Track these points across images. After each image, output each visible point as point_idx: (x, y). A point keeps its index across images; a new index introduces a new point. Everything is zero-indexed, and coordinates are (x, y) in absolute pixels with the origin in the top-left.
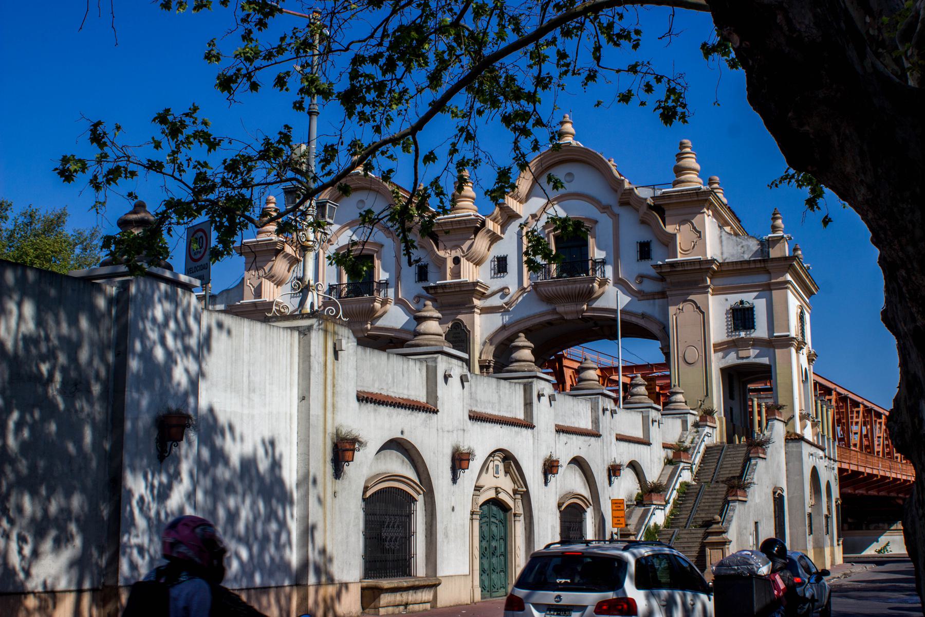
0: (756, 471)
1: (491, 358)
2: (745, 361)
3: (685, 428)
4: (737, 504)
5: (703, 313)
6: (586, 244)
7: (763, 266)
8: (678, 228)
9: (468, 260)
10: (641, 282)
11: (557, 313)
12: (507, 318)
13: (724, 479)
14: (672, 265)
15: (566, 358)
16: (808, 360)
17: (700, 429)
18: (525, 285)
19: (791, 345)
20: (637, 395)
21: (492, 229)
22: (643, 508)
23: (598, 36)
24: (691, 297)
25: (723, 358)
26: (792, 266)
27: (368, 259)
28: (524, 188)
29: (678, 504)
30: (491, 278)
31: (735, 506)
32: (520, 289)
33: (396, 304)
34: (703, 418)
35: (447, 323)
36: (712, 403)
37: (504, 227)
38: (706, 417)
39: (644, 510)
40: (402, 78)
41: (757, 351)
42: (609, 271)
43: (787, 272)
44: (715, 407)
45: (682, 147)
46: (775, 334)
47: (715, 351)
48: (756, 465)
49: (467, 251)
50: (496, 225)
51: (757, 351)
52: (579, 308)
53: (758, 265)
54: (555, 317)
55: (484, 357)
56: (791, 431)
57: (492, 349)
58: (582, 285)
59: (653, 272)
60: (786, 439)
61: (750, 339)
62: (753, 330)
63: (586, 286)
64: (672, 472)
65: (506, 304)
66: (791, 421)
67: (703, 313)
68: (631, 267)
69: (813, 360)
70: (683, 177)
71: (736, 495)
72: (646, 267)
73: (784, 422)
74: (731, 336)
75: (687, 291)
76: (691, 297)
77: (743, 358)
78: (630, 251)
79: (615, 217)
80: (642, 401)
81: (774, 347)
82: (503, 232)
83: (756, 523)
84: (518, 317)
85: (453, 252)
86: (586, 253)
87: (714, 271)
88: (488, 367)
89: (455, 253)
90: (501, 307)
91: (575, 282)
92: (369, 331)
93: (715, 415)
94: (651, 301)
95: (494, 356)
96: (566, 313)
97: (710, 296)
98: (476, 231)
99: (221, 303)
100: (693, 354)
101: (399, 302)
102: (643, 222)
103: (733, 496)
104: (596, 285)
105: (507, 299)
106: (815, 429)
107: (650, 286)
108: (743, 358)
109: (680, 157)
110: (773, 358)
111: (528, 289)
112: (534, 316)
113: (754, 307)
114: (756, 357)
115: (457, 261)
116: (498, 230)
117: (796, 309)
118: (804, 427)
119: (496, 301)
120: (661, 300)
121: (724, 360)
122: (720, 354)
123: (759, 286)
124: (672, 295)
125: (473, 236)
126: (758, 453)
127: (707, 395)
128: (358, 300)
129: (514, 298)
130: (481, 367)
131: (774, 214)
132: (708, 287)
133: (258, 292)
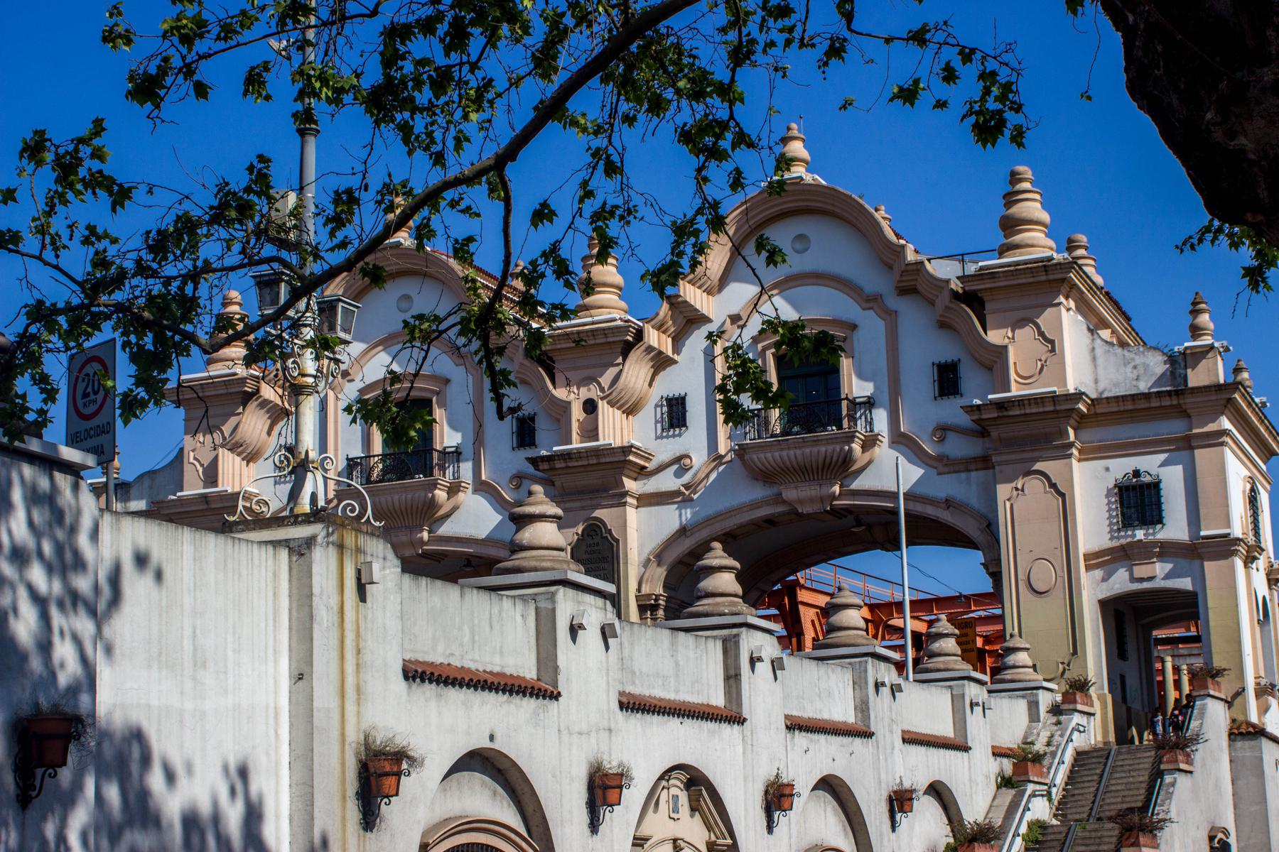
0: (1174, 797)
1: (659, 590)
2: (1146, 585)
3: (1034, 716)
7: (1175, 402)
8: (1010, 335)
9: (611, 404)
11: (784, 502)
12: (688, 514)
13: (1113, 813)
14: (1001, 405)
15: (803, 587)
16: (1269, 580)
17: (1063, 718)
19: (1235, 553)
21: (656, 345)
24: (1038, 466)
25: (1104, 580)
26: (1230, 401)
27: (419, 407)
30: (657, 438)
33: (475, 491)
34: (1068, 697)
37: (678, 340)
38: (1075, 694)
41: (1169, 566)
42: (881, 419)
43: (1222, 413)
44: (1091, 675)
45: (1015, 178)
46: (1203, 533)
47: (1088, 568)
48: (1173, 784)
49: (610, 387)
50: (663, 336)
51: (1169, 566)
52: (825, 491)
53: (1166, 402)
54: (780, 509)
55: (646, 589)
56: (1240, 718)
57: (661, 572)
60: (1231, 734)
62: (1159, 526)
65: (687, 487)
67: (1062, 495)
70: (1017, 238)
72: (951, 409)
73: (1226, 701)
74: (1118, 538)
76: (1038, 466)
77: (1141, 580)
78: (920, 381)
79: (890, 316)
80: (951, 666)
81: (1202, 558)
85: (583, 390)
88: (654, 608)
89: (585, 393)
90: (677, 493)
91: (817, 442)
92: (426, 544)
94: (963, 475)
95: (666, 587)
96: (801, 501)
97: (1074, 462)
98: (626, 349)
99: (140, 498)
100: (1045, 575)
101: (482, 487)
102: (943, 325)
104: (856, 447)
105: (687, 478)
107: (958, 447)
108: (1141, 580)
109: (1011, 198)
110: (1201, 579)
111: (728, 458)
112: (740, 509)
113: (1160, 481)
115: (590, 407)
116: (667, 346)
119: (667, 482)
120: (981, 473)
121: (1104, 584)
122: (1098, 573)
124: (1001, 463)
127: (1075, 652)
128: (404, 487)
130: (642, 609)
131: (1195, 304)
132: (1071, 445)
133: (211, 475)
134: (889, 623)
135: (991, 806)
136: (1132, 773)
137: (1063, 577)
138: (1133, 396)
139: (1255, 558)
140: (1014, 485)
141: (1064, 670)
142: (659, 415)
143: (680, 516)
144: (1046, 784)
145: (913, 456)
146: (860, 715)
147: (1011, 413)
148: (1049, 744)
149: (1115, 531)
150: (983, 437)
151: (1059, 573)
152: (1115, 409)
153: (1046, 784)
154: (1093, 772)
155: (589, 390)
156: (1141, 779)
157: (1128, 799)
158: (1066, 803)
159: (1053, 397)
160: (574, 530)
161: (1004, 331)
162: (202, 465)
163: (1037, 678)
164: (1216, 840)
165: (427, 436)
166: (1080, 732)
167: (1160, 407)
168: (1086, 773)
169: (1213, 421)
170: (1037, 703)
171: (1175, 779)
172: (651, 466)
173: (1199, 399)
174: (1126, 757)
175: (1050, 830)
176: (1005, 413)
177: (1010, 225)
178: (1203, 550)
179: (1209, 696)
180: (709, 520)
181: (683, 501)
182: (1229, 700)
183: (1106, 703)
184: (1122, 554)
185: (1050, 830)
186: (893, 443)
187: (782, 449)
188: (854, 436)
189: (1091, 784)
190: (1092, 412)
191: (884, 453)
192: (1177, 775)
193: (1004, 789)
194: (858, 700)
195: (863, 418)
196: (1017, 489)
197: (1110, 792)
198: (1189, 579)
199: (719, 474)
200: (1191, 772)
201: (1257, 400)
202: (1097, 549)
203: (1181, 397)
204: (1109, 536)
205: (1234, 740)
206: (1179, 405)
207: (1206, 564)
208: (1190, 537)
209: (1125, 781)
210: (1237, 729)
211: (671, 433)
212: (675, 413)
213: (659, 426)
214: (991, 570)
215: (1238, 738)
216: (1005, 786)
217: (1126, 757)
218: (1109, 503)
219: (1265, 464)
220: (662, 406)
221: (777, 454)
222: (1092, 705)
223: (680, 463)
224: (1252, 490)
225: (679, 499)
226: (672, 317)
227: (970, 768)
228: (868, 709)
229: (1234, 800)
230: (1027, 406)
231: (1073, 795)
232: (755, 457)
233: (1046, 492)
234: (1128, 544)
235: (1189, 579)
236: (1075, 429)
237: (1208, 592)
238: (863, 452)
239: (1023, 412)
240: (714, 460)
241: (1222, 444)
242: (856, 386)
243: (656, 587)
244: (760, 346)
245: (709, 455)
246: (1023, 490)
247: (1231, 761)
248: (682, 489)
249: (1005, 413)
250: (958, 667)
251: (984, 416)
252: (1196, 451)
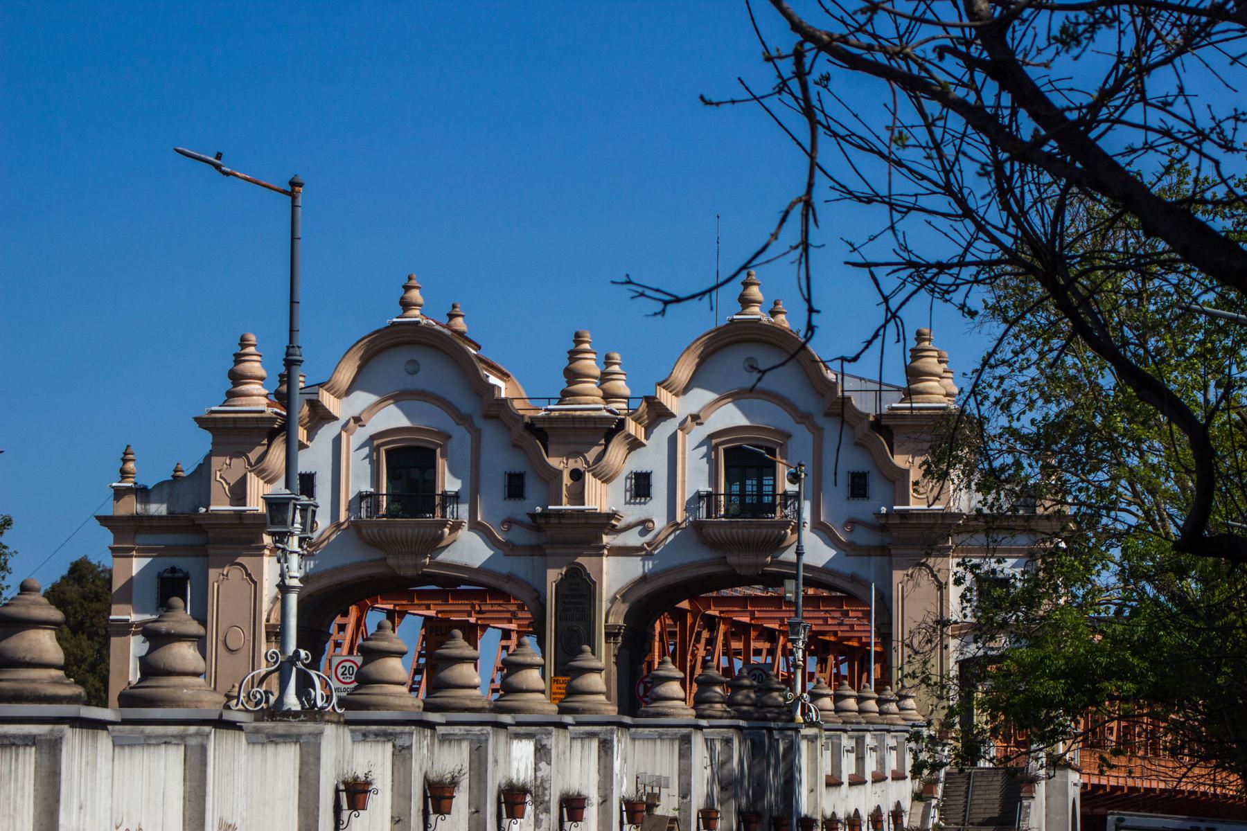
1: (621, 623)
6: (433, 466)
8: (911, 460)
9: (595, 476)
11: (726, 564)
12: (649, 565)
13: (980, 820)
18: (679, 520)
21: (633, 433)
23: (899, 163)
24: (239, 560)
28: (685, 376)
30: (626, 503)
32: (671, 524)
33: (470, 529)
35: (561, 568)
40: (890, 192)
42: (463, 510)
45: (243, 343)
46: (111, 617)
48: (1029, 807)
50: (639, 426)
54: (722, 569)
55: (611, 621)
57: (623, 608)
58: (770, 531)
59: (870, 518)
63: (433, 531)
65: (649, 544)
67: (255, 583)
68: (495, 504)
70: (921, 386)
72: (518, 509)
76: (239, 560)
78: (494, 485)
79: (817, 431)
82: (647, 437)
84: (667, 565)
85: (571, 461)
86: (432, 483)
88: (616, 635)
89: (573, 464)
90: (641, 548)
91: (760, 525)
92: (426, 567)
94: (865, 559)
95: (625, 620)
97: (266, 559)
98: (609, 435)
99: (161, 502)
100: (238, 638)
101: (475, 526)
102: (515, 446)
104: (447, 530)
105: (649, 537)
107: (863, 537)
109: (239, 358)
111: (684, 525)
115: (577, 475)
119: (632, 539)
120: (879, 558)
125: (603, 441)
128: (419, 524)
129: (661, 537)
130: (608, 635)
131: (125, 454)
142: (628, 486)
143: (644, 566)
145: (829, 541)
155: (576, 462)
156: (995, 797)
157: (988, 811)
160: (559, 571)
161: (907, 456)
162: (228, 484)
165: (431, 482)
172: (619, 525)
177: (237, 378)
180: (666, 572)
191: (810, 539)
199: (675, 537)
211: (638, 501)
212: (641, 486)
213: (628, 494)
220: (631, 478)
221: (728, 531)
223: (645, 525)
226: (648, 413)
232: (711, 531)
233: (243, 579)
242: (449, 483)
243: (618, 619)
244: (714, 442)
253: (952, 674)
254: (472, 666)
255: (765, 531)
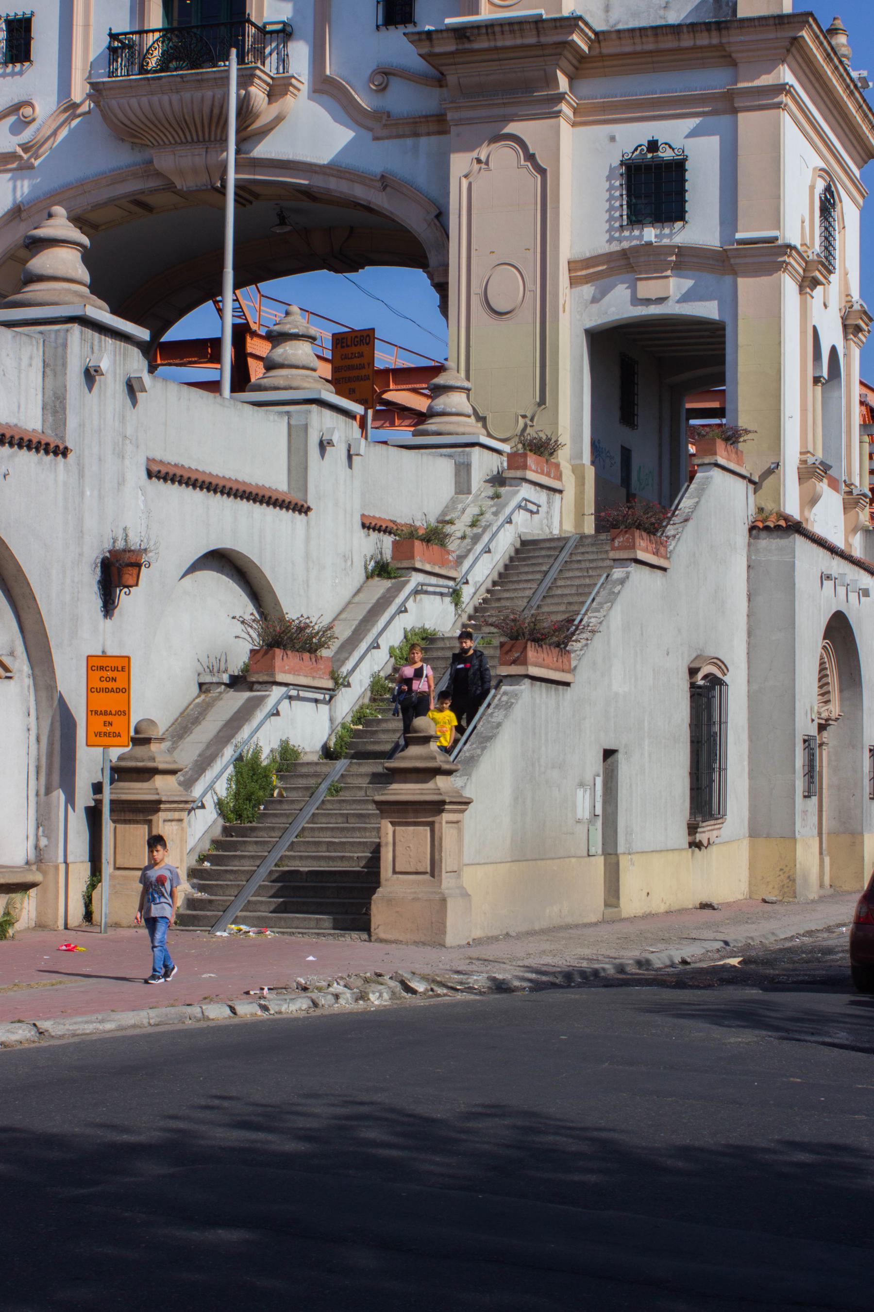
0: (620, 599)
2: (654, 310)
3: (463, 486)
4: (525, 686)
5: (542, 171)
7: (715, 41)
10: (382, 89)
11: (158, 174)
14: (461, 33)
15: (254, 334)
16: (845, 327)
17: (503, 490)
19: (781, 267)
20: (282, 366)
22: (247, 694)
25: (595, 300)
26: (796, 41)
29: (383, 687)
31: (516, 695)
32: (65, 103)
34: (516, 461)
36: (556, 423)
38: (525, 455)
39: (249, 700)
41: (688, 283)
43: (783, 61)
44: (565, 436)
46: (739, 236)
47: (574, 282)
48: (622, 582)
51: (688, 283)
53: (703, 40)
54: (152, 184)
56: (769, 506)
60: (752, 529)
61: (669, 250)
62: (679, 224)
64: (383, 597)
65: (26, 148)
66: (771, 479)
69: (858, 329)
71: (522, 661)
73: (751, 481)
74: (620, 240)
75: (496, 111)
76: (512, 128)
77: (648, 302)
80: (295, 384)
81: (735, 272)
83: (609, 754)
87: (582, 58)
93: (563, 457)
94: (409, 142)
97: (564, 126)
103: (514, 662)
105: (27, 135)
106: (852, 513)
108: (648, 302)
110: (731, 303)
111: (85, 108)
113: (685, 160)
114: (685, 298)
117: (809, 174)
118: (811, 500)
120: (434, 139)
121: (595, 307)
122: (588, 290)
123: (702, 100)
124: (460, 123)
126: (633, 547)
127: (542, 402)
132: (560, 98)
134: (385, 396)
135: (349, 603)
136: (591, 573)
137: (534, 292)
138: (655, 29)
139: (815, 283)
140: (474, 154)
141: (526, 426)
143: (14, 189)
144: (454, 579)
146: (50, 419)
147: (476, 46)
148: (473, 525)
149: (616, 230)
150: (441, 86)
151: (529, 286)
152: (628, 49)
153: (454, 579)
154: (537, 569)
158: (485, 610)
159: (536, 22)
163: (471, 429)
164: (700, 675)
166: (531, 512)
167: (694, 48)
168: (526, 569)
169: (769, 72)
170: (468, 466)
171: (628, 573)
173: (747, 38)
174: (590, 549)
175: (440, 644)
176: (467, 46)
178: (738, 261)
179: (717, 465)
181: (20, 168)
182: (756, 479)
183: (583, 478)
184: (623, 262)
185: (440, 644)
186: (315, 91)
187: (152, 93)
188: (253, 76)
189: (529, 585)
190: (596, 52)
192: (633, 568)
193: (377, 579)
194: (49, 393)
195: (274, 55)
196: (479, 161)
197: (552, 596)
198: (715, 304)
199: (70, 131)
200: (664, 569)
201: (854, 74)
202: (588, 255)
203: (724, 32)
204: (607, 236)
205: (757, 538)
206: (721, 46)
207: (740, 281)
208: (722, 241)
209: (577, 582)
210: (763, 521)
214: (436, 281)
215: (763, 534)
216: (379, 575)
217: (590, 549)
218: (611, 188)
219: (859, 168)
221: (144, 100)
222: (559, 477)
224: (828, 189)
225: (14, 166)
227: (308, 539)
228: (64, 409)
229: (748, 623)
230: (499, 35)
231: (499, 600)
232: (114, 103)
234: (631, 248)
235: (715, 304)
236: (571, 79)
237: (740, 322)
238: (270, 103)
239: (492, 44)
240: (65, 110)
241: (778, 106)
245: (59, 102)
246: (487, 163)
247: (749, 567)
248: (19, 151)
249: (467, 46)
250: (306, 385)
251: (438, 50)
252: (741, 116)
253: (464, 645)
254: (464, 396)
255: (209, 94)
